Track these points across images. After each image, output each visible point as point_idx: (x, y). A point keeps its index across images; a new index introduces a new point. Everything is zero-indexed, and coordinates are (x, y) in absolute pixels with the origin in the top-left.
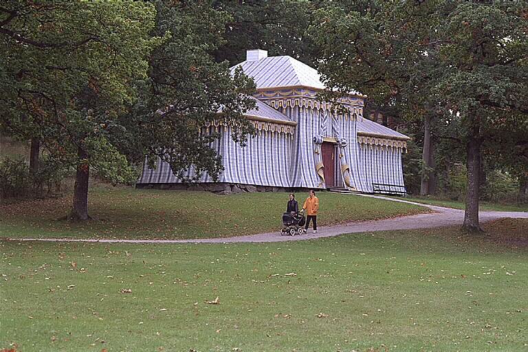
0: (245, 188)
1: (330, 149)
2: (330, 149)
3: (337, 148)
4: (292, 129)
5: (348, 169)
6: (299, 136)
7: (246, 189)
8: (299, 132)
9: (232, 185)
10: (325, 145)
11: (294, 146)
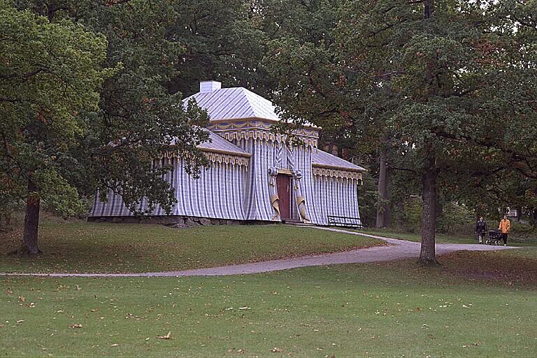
0: (198, 220)
1: (285, 181)
2: (285, 181)
3: (292, 180)
4: (246, 160)
5: (304, 201)
6: (253, 168)
7: (199, 222)
8: (253, 164)
9: (185, 218)
10: (280, 177)
11: (248, 178)
